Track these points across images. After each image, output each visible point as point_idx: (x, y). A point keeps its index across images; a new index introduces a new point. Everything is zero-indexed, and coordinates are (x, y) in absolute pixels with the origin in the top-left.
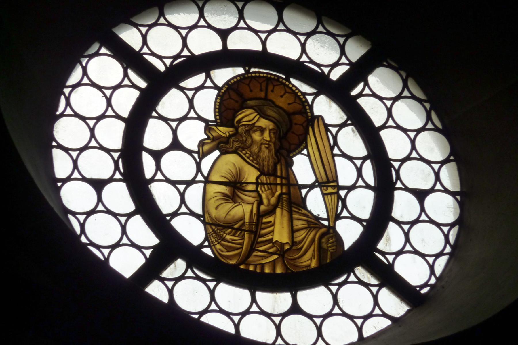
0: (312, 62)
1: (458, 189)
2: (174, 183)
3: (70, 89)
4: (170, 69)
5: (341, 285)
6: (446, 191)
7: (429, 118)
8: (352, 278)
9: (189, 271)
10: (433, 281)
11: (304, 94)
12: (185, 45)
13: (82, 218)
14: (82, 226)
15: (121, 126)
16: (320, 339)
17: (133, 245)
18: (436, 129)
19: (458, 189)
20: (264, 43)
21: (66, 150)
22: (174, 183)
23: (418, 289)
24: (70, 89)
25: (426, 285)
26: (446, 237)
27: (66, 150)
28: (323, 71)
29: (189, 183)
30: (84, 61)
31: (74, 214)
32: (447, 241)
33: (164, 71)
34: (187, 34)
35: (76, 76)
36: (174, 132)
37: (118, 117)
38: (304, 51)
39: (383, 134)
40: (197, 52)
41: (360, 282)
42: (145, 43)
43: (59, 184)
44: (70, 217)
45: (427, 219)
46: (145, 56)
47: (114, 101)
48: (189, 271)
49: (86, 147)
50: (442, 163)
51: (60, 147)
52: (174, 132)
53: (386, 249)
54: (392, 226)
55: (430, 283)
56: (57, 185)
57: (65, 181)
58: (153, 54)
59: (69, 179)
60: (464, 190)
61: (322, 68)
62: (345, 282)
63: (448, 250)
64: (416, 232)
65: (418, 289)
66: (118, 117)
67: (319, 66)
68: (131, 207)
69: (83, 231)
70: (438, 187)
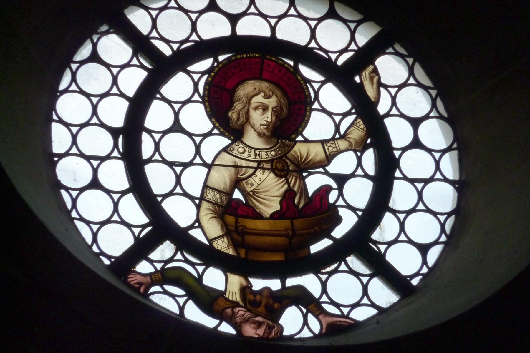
0: (321, 48)
1: (457, 178)
2: (171, 165)
3: (78, 65)
4: (177, 54)
5: (331, 274)
6: (446, 180)
7: (434, 106)
8: (343, 267)
9: (179, 253)
10: (425, 270)
11: (309, 81)
12: (194, 29)
13: (74, 194)
14: (74, 201)
15: (125, 105)
16: (306, 327)
17: (123, 222)
18: (441, 117)
19: (457, 178)
20: (273, 29)
21: (67, 125)
22: (171, 165)
23: (408, 279)
24: (78, 65)
25: (417, 274)
26: (443, 226)
27: (67, 125)
28: (330, 58)
29: (186, 165)
30: (95, 38)
31: (67, 189)
32: (443, 230)
33: (170, 56)
34: (91, 118)
35: (85, 52)
36: (177, 114)
37: (122, 95)
38: (313, 36)
39: (387, 121)
40: (206, 36)
41: (351, 272)
42: (154, 26)
43: (56, 159)
44: (63, 192)
45: (434, 153)
46: (152, 41)
47: (120, 80)
48: (179, 253)
49: (82, 126)
50: (444, 152)
51: (61, 121)
52: (177, 114)
53: (380, 236)
54: (388, 216)
55: (421, 272)
56: (53, 159)
57: (61, 156)
58: (162, 39)
59: (67, 154)
60: (463, 178)
61: (330, 54)
62: (335, 271)
63: (443, 238)
64: (412, 222)
65: (408, 279)
66: (122, 95)
67: (326, 52)
68: (125, 185)
69: (74, 206)
70: (438, 176)
